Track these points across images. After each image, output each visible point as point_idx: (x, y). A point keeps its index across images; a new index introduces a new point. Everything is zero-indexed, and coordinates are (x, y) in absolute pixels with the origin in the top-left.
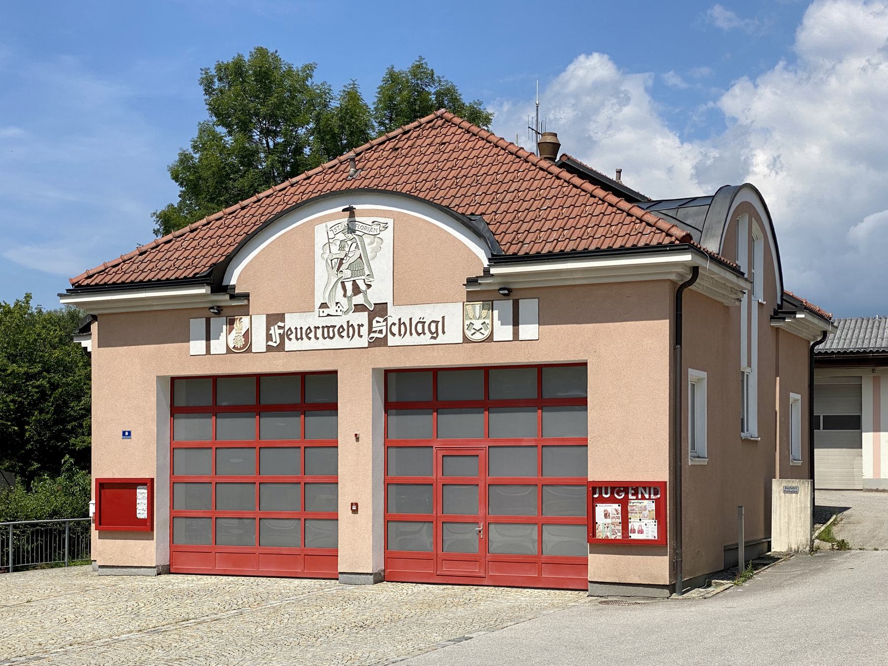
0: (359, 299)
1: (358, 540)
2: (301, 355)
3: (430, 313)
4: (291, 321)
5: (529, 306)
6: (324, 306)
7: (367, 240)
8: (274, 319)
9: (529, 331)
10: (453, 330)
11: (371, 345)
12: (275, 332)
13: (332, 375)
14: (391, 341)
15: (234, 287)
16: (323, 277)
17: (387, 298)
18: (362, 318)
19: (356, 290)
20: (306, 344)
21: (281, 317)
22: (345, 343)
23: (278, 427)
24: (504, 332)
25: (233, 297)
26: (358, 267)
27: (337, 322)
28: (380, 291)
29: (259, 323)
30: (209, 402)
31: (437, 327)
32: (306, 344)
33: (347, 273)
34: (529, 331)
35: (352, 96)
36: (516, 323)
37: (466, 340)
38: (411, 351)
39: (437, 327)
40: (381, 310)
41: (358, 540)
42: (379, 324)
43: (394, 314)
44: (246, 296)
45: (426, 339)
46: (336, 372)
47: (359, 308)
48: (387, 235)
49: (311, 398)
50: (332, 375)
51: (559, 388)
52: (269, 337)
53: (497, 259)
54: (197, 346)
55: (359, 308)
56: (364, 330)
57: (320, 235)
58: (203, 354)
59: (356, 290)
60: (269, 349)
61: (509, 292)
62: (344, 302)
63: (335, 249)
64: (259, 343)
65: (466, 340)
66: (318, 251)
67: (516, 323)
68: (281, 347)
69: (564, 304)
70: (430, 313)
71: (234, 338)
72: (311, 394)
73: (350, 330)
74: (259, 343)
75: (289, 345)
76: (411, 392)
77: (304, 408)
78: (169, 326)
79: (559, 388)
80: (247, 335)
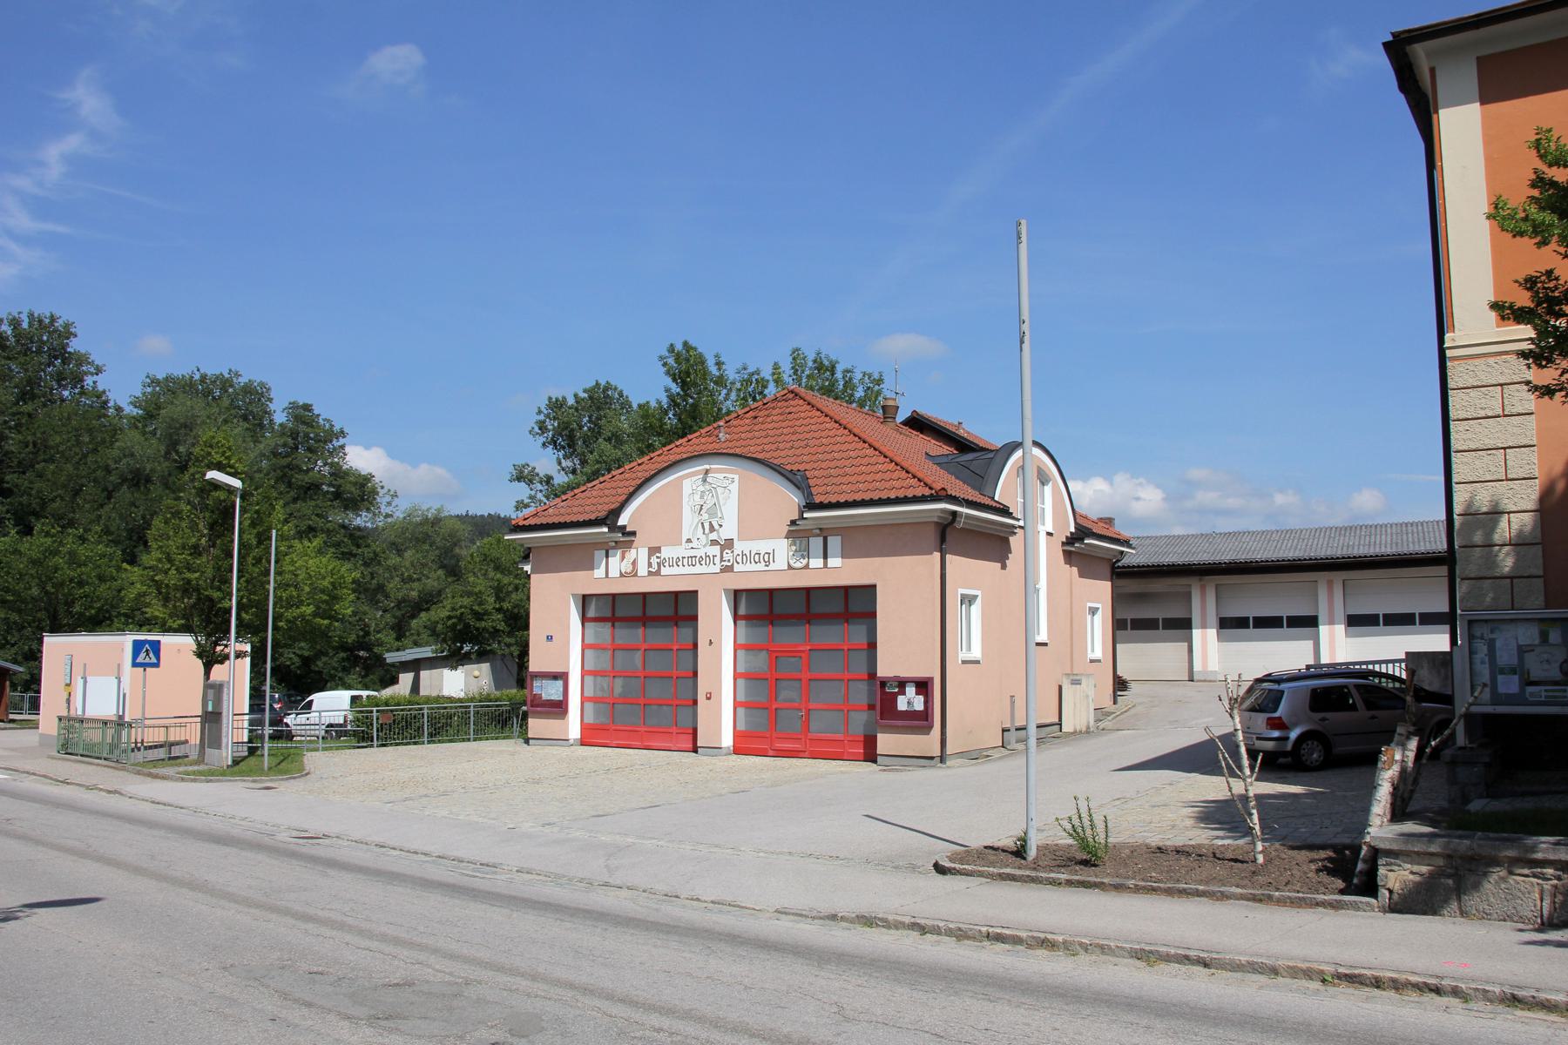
0: (714, 536)
1: (721, 716)
2: (672, 579)
3: (763, 546)
4: (666, 552)
5: (835, 542)
6: (689, 541)
7: (720, 490)
8: (654, 551)
9: (834, 562)
10: (775, 562)
11: (722, 571)
12: (654, 560)
13: (693, 594)
14: (737, 568)
15: (624, 527)
16: (689, 522)
17: (735, 537)
18: (716, 550)
19: (712, 529)
20: (675, 570)
21: (658, 550)
22: (698, 569)
23: (828, 634)
24: (816, 563)
25: (1528, 383)
26: (713, 511)
27: (698, 553)
28: (729, 530)
29: (643, 554)
30: (802, 610)
31: (769, 558)
32: (675, 570)
33: (706, 516)
34: (834, 562)
35: (659, 402)
36: (825, 557)
37: (790, 567)
38: (754, 576)
39: (769, 558)
40: (729, 544)
41: (721, 716)
42: (728, 555)
43: (739, 547)
44: (633, 533)
45: (761, 567)
46: (874, 586)
47: (714, 543)
48: (735, 487)
49: (853, 608)
50: (693, 594)
51: (855, 605)
52: (650, 565)
53: (811, 506)
54: (599, 573)
55: (714, 543)
56: (717, 560)
57: (687, 485)
58: (614, 573)
59: (712, 529)
60: (650, 573)
61: (824, 533)
62: (703, 538)
63: (697, 497)
64: (643, 570)
65: (790, 567)
66: (685, 499)
67: (825, 557)
68: (658, 573)
69: (859, 541)
70: (763, 546)
71: (626, 566)
72: (677, 610)
73: (708, 559)
74: (643, 570)
75: (664, 571)
76: (763, 608)
77: (847, 616)
78: (581, 556)
79: (855, 605)
80: (634, 563)
